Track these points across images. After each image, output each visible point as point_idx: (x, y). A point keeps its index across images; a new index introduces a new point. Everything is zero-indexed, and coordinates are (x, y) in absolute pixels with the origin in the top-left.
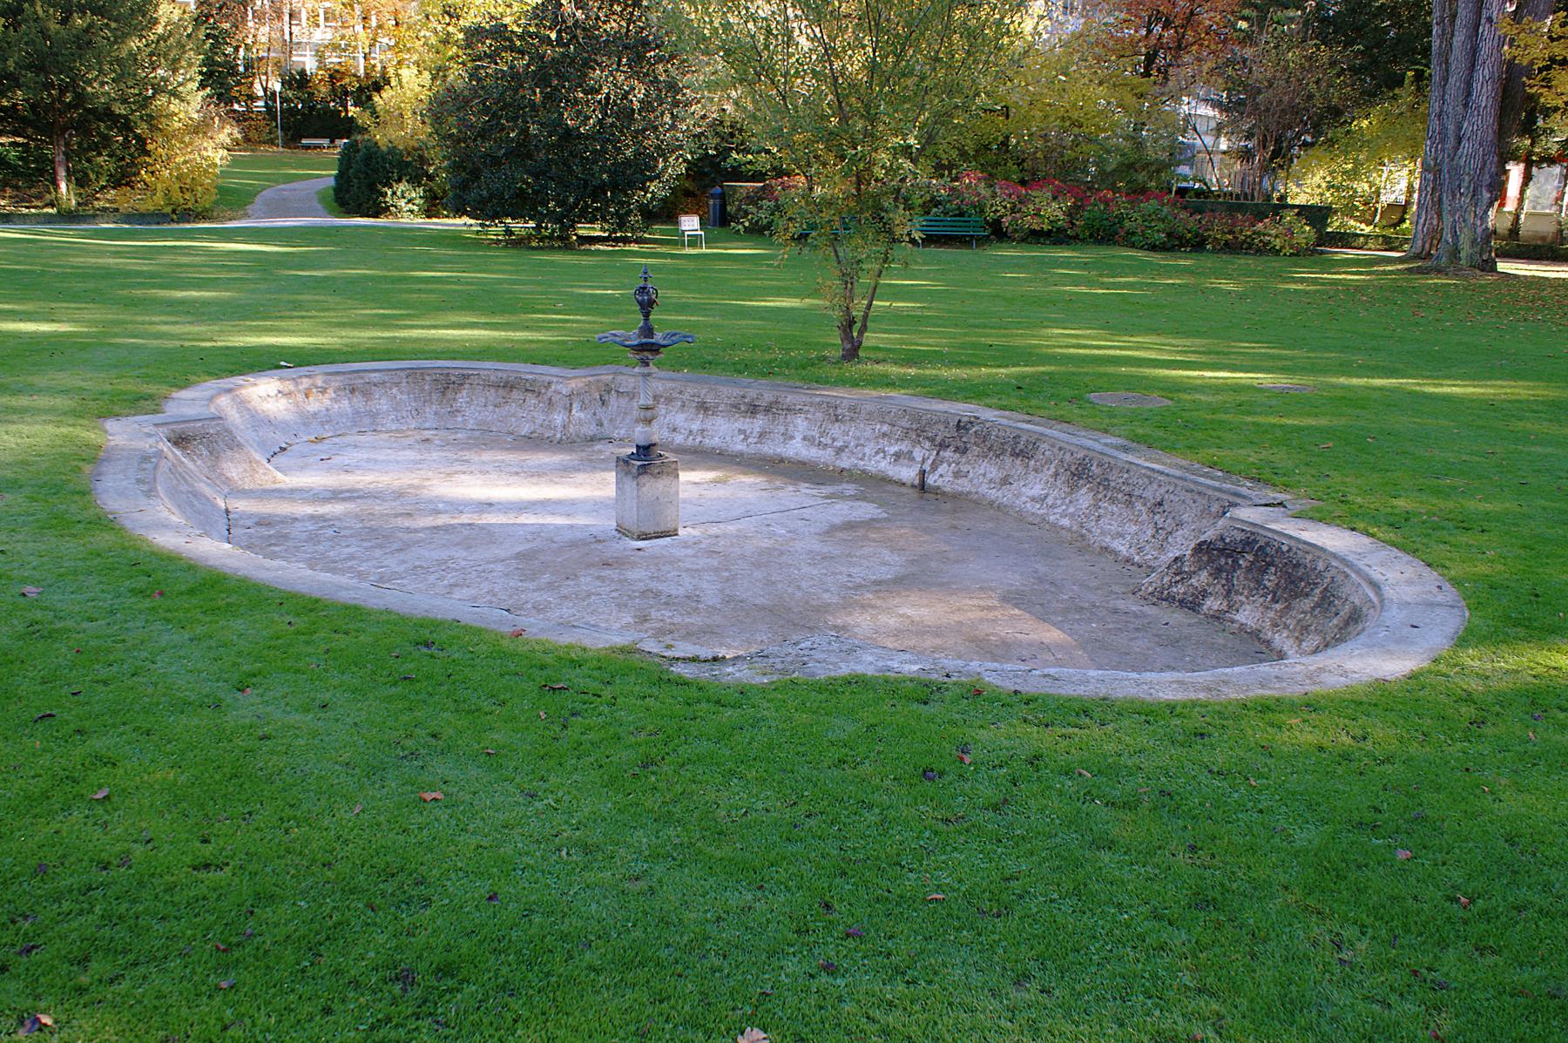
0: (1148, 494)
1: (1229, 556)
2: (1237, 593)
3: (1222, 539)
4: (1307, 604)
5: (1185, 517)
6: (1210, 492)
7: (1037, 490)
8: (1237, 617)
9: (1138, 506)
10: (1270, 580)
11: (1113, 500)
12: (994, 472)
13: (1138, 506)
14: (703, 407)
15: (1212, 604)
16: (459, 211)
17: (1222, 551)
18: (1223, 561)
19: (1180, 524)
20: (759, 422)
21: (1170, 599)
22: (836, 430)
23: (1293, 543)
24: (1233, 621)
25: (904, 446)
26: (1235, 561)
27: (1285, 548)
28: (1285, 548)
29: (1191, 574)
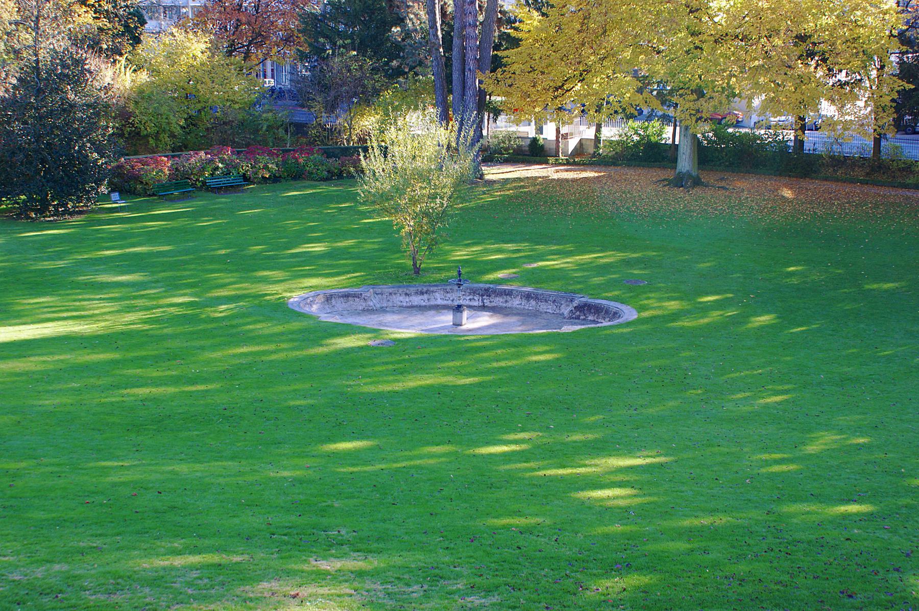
7: (518, 302)
12: (501, 300)
14: (406, 294)
20: (426, 297)
22: (449, 295)
25: (471, 297)
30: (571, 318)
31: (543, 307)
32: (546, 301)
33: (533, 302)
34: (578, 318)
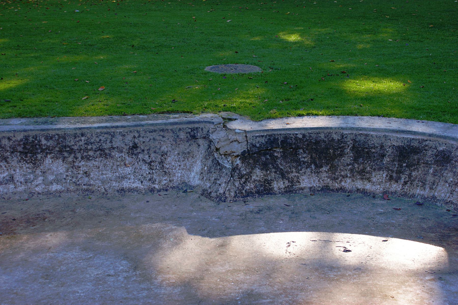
0: (118, 142)
1: (265, 155)
2: (288, 172)
3: (254, 146)
4: (347, 159)
5: (164, 148)
6: (170, 127)
8: (302, 185)
9: (116, 154)
10: (304, 157)
11: (88, 158)
13: (116, 154)
15: (279, 185)
16: (383, 73)
17: (259, 153)
18: (263, 158)
19: (164, 154)
21: (249, 194)
23: (303, 132)
24: (302, 189)
26: (272, 155)
27: (301, 136)
28: (301, 136)
29: (249, 174)
30: (244, 195)
31: (101, 174)
32: (104, 153)
33: (56, 167)
34: (265, 190)
